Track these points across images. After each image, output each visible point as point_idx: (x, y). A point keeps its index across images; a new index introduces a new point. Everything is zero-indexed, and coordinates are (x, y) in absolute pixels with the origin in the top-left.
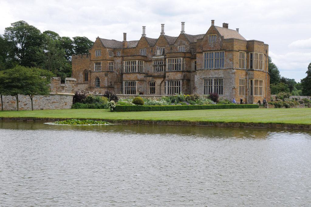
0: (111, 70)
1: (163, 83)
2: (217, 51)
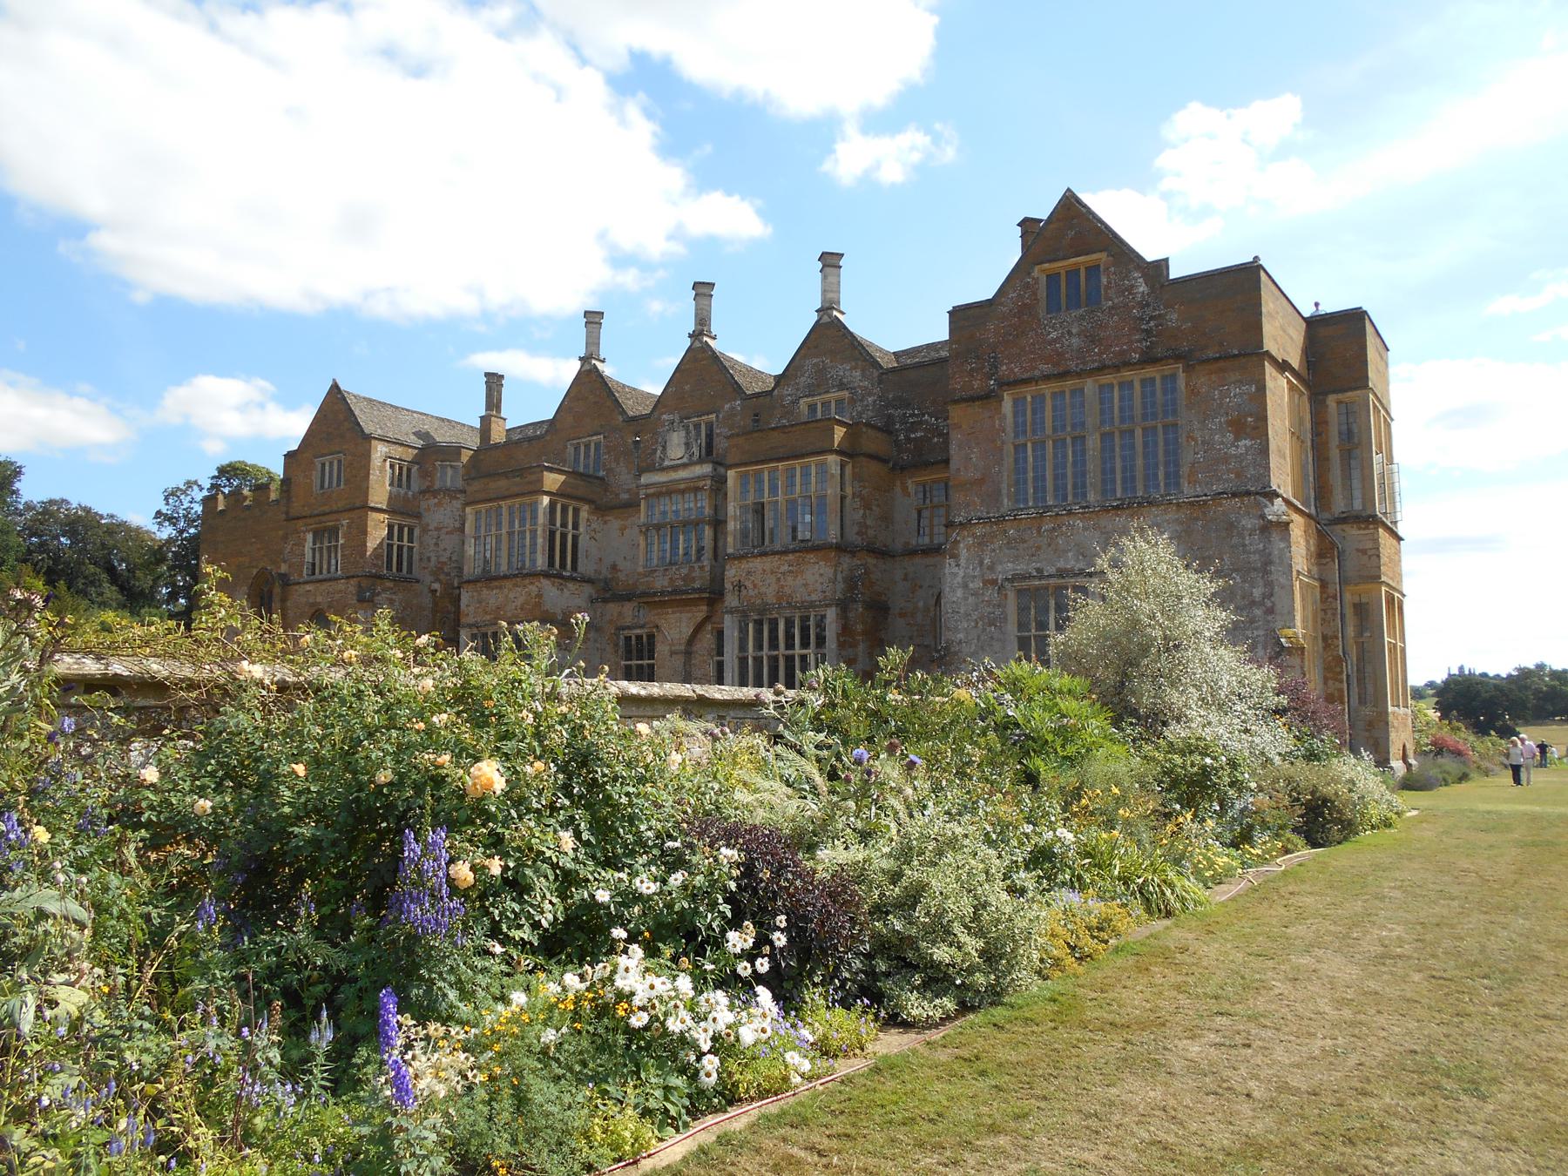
0: (399, 569)
1: (707, 639)
2: (1117, 368)
